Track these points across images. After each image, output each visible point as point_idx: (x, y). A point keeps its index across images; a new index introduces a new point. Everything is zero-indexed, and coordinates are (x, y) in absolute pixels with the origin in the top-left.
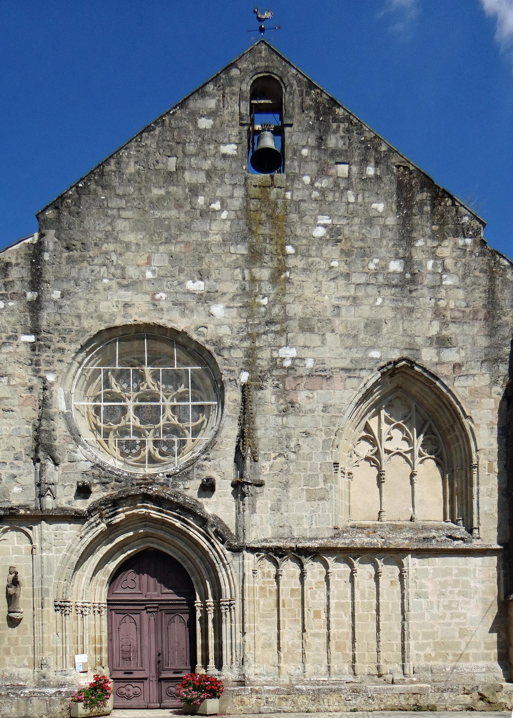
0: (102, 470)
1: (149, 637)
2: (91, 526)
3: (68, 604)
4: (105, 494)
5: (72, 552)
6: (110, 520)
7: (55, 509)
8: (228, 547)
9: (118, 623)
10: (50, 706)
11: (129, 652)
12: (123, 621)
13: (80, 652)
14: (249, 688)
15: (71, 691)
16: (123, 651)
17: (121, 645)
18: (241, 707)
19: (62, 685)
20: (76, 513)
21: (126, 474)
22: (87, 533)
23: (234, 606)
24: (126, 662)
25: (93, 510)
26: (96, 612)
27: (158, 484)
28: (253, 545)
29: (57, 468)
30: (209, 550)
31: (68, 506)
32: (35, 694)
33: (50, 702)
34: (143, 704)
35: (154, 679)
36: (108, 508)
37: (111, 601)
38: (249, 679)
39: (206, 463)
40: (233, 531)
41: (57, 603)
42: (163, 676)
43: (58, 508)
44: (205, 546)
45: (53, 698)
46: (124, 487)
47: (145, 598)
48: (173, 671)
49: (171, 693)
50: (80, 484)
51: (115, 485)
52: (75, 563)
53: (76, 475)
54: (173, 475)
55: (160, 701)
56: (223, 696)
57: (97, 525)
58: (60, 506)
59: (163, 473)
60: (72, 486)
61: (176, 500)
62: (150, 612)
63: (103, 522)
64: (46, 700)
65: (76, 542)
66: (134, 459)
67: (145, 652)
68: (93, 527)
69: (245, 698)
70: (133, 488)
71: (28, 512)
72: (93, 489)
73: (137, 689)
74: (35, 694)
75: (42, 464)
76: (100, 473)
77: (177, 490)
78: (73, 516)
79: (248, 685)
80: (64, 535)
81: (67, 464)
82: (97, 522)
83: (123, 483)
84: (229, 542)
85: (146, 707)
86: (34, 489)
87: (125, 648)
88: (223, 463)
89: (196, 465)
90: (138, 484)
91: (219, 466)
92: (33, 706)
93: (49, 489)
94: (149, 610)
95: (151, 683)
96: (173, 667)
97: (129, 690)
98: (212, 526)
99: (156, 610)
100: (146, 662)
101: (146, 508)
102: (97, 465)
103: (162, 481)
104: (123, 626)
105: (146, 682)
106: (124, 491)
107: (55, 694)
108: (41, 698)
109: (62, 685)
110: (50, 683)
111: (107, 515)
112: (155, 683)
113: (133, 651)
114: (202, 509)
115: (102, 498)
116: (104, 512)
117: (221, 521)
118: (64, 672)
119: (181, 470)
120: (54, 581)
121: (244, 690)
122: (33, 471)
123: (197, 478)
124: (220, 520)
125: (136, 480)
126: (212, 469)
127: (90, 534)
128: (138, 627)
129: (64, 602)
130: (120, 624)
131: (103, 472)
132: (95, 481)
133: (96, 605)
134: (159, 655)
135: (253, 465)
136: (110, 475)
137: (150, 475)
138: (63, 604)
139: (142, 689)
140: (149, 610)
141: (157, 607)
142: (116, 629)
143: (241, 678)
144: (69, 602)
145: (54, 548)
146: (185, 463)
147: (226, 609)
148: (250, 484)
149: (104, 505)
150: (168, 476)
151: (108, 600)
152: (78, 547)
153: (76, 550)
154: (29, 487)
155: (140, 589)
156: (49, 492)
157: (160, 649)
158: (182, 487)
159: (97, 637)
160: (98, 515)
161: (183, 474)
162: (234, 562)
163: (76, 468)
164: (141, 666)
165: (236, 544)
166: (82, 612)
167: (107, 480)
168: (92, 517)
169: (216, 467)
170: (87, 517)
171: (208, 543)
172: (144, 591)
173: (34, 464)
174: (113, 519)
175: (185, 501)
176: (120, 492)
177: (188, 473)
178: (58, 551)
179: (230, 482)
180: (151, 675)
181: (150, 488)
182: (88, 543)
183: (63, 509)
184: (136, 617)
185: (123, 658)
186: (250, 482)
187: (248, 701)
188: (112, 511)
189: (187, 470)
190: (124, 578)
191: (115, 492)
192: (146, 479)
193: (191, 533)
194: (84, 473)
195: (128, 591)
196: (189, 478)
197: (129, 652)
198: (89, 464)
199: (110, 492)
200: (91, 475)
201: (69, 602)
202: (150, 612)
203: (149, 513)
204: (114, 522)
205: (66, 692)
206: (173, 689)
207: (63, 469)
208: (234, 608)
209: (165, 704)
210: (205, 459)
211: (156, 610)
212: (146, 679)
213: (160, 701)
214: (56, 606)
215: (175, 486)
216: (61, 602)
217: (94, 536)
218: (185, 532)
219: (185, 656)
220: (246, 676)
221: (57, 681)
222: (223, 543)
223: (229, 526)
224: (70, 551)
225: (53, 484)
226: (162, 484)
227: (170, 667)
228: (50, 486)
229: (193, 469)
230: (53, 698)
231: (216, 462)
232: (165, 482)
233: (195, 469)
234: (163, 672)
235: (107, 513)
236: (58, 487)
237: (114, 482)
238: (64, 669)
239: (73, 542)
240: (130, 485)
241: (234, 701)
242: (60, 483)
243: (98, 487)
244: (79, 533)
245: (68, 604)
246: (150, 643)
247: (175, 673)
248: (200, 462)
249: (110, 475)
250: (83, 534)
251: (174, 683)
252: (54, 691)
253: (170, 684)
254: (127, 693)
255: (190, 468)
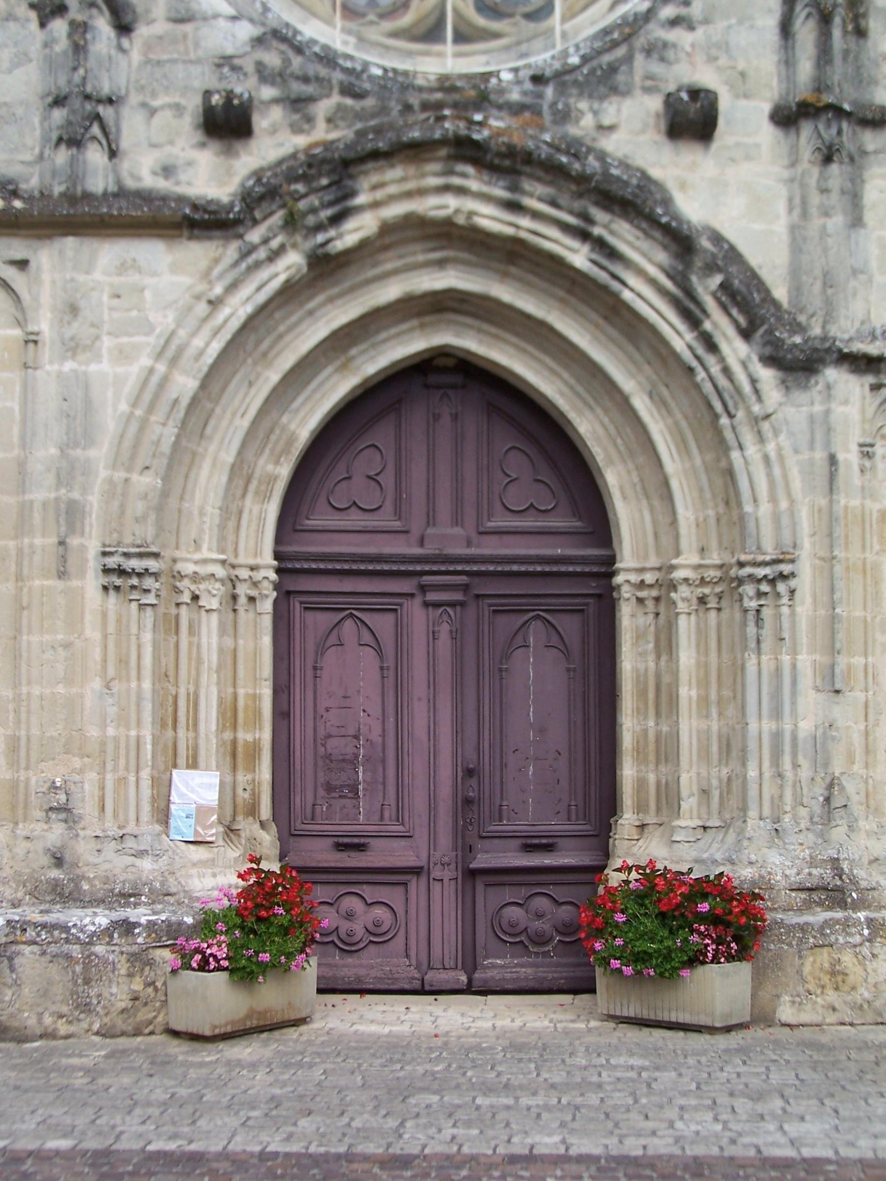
0: (291, 54)
1: (433, 708)
2: (251, 260)
3: (152, 565)
4: (301, 141)
5: (174, 362)
6: (320, 238)
7: (116, 195)
8: (768, 350)
9: (311, 647)
10: (87, 982)
11: (353, 762)
12: (333, 639)
13: (182, 761)
14: (862, 915)
15: (168, 923)
16: (328, 757)
17: (321, 733)
18: (831, 996)
19: (128, 897)
20: (195, 207)
21: (379, 72)
22: (232, 287)
23: (793, 583)
24: (338, 804)
25: (262, 198)
26: (242, 600)
27: (500, 107)
28: (859, 347)
29: (125, 42)
30: (694, 363)
31: (162, 185)
32: (31, 933)
33: (86, 968)
34: (407, 973)
35: (447, 874)
36: (311, 191)
37: (298, 557)
38: (854, 881)
39: (678, 36)
40: (780, 293)
41: (112, 562)
42: (482, 860)
43: (121, 193)
44: (679, 345)
45: (99, 949)
46: (373, 116)
47: (417, 551)
48: (517, 843)
49: (513, 929)
50: (216, 99)
51: (339, 107)
52: (185, 402)
53: (196, 70)
54: (558, 75)
55: (470, 964)
56: (770, 946)
57: (274, 255)
58: (130, 184)
59: (516, 70)
60: (178, 109)
61: (577, 166)
62: (436, 605)
63: (294, 246)
64: (68, 957)
65: (191, 322)
66: (388, 25)
67: (417, 768)
68: (258, 265)
69: (847, 959)
70: (411, 119)
71: (18, 204)
72: (261, 122)
73: (379, 912)
74: (31, 933)
75: (73, 24)
76: (287, 62)
77: (573, 131)
78: (186, 217)
79: (857, 906)
80: (148, 294)
81: (161, 27)
82: (275, 244)
83: (370, 102)
84: (770, 332)
85: (416, 984)
86: (36, 120)
87: (338, 746)
88: (741, 38)
89: (640, 41)
90: (426, 106)
91: (725, 46)
92: (17, 984)
93: (98, 117)
94: (432, 597)
95: (436, 887)
96: (521, 826)
97: (350, 916)
98: (711, 268)
99: (458, 596)
100: (418, 802)
101: (461, 191)
102: (276, 34)
103: (515, 96)
104: (331, 658)
105: (416, 886)
106: (378, 131)
107: (108, 932)
108: (53, 949)
109: (128, 897)
110: (77, 887)
111: (311, 220)
112: (450, 889)
113: (368, 759)
114: (667, 202)
115: (294, 156)
116: (302, 205)
117: (733, 255)
118: (130, 843)
119: (585, 59)
120: (103, 473)
121: (846, 924)
122: (35, 49)
123: (647, 90)
124: (732, 248)
125: (421, 89)
126: (700, 58)
127: (246, 290)
128: (390, 662)
129: (141, 555)
130: (321, 650)
131: (297, 61)
132: (268, 92)
133: (244, 574)
134: (470, 772)
135: (853, 46)
136: (323, 72)
137: (468, 77)
138: (135, 564)
139: (400, 909)
140: (432, 597)
141: (466, 588)
142: (303, 670)
143: (822, 874)
144: (156, 555)
145: (107, 342)
146: (595, 37)
147: (760, 595)
148: (849, 115)
149: (304, 178)
150: (538, 79)
151: (277, 556)
152: (198, 342)
153: (191, 351)
154: (20, 111)
155: (398, 513)
156: (96, 130)
157: (471, 755)
158: (588, 121)
159: (241, 703)
160: (277, 218)
161: (593, 72)
162: (789, 412)
163: (197, 45)
164: (399, 819)
165: (798, 339)
166: (195, 598)
167: (309, 89)
168: (255, 222)
169: (714, 52)
170: (237, 222)
171: (690, 336)
172: (416, 527)
173: (43, 25)
174: (332, 233)
175: (606, 174)
176: (361, 134)
177: (613, 69)
178: (123, 355)
179: (766, 108)
180: (437, 856)
181: (478, 117)
182: (235, 324)
183: (145, 197)
184: (383, 624)
185: (329, 788)
186: (847, 107)
187: (859, 969)
188: (331, 204)
189: (607, 58)
190: (340, 471)
191: (342, 134)
192: (453, 89)
193: (627, 295)
194: (225, 62)
195: (355, 520)
196: (615, 90)
197: (353, 762)
198: (246, 31)
199: (321, 133)
200: (250, 68)
201: (156, 555)
202: (436, 605)
203: (471, 214)
204: (339, 245)
205: (151, 924)
206: (514, 913)
207: (148, 47)
208: (792, 592)
209: (490, 974)
210: (674, 22)
211: (458, 596)
212: (416, 871)
213: (470, 964)
214: (107, 571)
215: (564, 116)
216: (126, 555)
217: (262, 297)
218: (605, 289)
219: (564, 783)
220: (845, 866)
221: (106, 880)
222: (746, 334)
223: (765, 274)
224: (170, 353)
225: (110, 101)
226: (517, 109)
227: (505, 827)
228: (101, 109)
229: (629, 59)
230: (99, 949)
231: (716, 30)
232: (528, 100)
233: (639, 59)
234: (479, 845)
235: (313, 211)
236: (126, 112)
237: (336, 98)
238: (131, 828)
239: (179, 324)
240: (396, 108)
241: (807, 969)
242: (134, 99)
243: (277, 113)
244: (200, 288)
245: (152, 565)
246: (433, 733)
247: (529, 848)
248: (656, 32)
249: (323, 72)
250: (218, 290)
251: (524, 892)
252: (103, 919)
253: (508, 894)
254: (344, 926)
255: (621, 52)
